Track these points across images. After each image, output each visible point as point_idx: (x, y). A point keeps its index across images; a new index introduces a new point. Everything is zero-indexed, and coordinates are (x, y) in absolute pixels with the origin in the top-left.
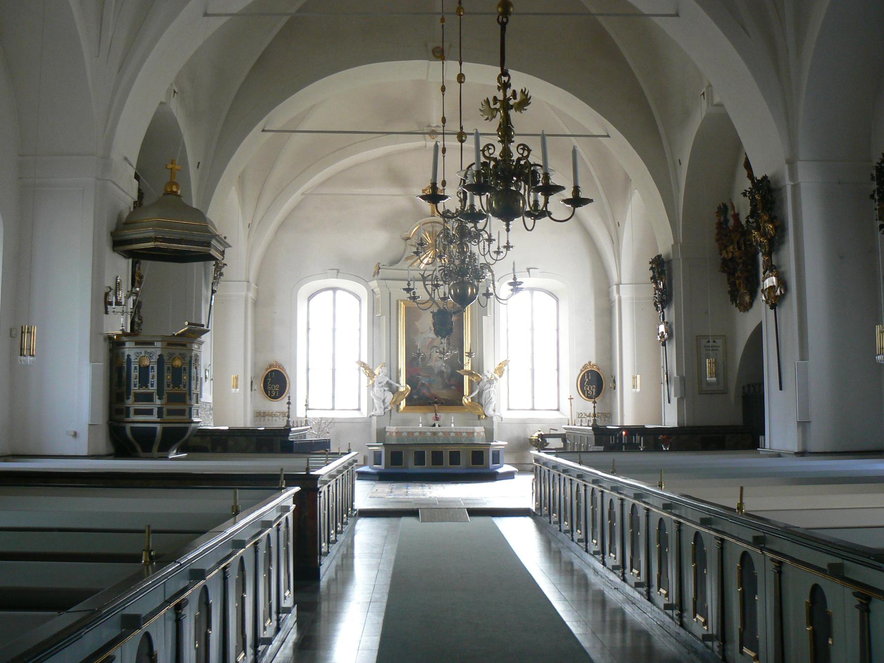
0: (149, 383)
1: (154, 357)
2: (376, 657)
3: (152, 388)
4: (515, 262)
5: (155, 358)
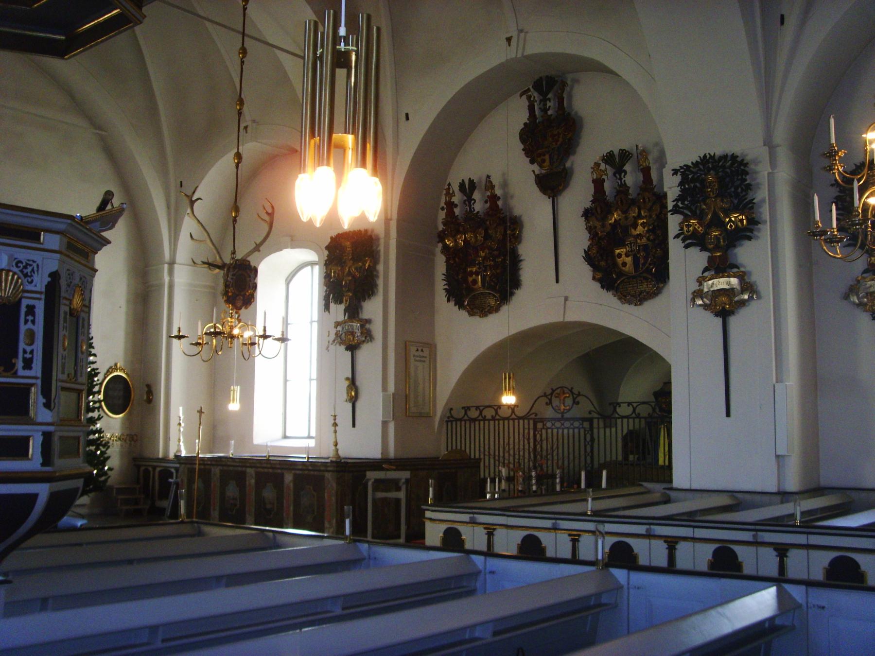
0: (17, 357)
1: (36, 278)
2: (259, 584)
3: (27, 373)
4: (266, 311)
5: (40, 282)
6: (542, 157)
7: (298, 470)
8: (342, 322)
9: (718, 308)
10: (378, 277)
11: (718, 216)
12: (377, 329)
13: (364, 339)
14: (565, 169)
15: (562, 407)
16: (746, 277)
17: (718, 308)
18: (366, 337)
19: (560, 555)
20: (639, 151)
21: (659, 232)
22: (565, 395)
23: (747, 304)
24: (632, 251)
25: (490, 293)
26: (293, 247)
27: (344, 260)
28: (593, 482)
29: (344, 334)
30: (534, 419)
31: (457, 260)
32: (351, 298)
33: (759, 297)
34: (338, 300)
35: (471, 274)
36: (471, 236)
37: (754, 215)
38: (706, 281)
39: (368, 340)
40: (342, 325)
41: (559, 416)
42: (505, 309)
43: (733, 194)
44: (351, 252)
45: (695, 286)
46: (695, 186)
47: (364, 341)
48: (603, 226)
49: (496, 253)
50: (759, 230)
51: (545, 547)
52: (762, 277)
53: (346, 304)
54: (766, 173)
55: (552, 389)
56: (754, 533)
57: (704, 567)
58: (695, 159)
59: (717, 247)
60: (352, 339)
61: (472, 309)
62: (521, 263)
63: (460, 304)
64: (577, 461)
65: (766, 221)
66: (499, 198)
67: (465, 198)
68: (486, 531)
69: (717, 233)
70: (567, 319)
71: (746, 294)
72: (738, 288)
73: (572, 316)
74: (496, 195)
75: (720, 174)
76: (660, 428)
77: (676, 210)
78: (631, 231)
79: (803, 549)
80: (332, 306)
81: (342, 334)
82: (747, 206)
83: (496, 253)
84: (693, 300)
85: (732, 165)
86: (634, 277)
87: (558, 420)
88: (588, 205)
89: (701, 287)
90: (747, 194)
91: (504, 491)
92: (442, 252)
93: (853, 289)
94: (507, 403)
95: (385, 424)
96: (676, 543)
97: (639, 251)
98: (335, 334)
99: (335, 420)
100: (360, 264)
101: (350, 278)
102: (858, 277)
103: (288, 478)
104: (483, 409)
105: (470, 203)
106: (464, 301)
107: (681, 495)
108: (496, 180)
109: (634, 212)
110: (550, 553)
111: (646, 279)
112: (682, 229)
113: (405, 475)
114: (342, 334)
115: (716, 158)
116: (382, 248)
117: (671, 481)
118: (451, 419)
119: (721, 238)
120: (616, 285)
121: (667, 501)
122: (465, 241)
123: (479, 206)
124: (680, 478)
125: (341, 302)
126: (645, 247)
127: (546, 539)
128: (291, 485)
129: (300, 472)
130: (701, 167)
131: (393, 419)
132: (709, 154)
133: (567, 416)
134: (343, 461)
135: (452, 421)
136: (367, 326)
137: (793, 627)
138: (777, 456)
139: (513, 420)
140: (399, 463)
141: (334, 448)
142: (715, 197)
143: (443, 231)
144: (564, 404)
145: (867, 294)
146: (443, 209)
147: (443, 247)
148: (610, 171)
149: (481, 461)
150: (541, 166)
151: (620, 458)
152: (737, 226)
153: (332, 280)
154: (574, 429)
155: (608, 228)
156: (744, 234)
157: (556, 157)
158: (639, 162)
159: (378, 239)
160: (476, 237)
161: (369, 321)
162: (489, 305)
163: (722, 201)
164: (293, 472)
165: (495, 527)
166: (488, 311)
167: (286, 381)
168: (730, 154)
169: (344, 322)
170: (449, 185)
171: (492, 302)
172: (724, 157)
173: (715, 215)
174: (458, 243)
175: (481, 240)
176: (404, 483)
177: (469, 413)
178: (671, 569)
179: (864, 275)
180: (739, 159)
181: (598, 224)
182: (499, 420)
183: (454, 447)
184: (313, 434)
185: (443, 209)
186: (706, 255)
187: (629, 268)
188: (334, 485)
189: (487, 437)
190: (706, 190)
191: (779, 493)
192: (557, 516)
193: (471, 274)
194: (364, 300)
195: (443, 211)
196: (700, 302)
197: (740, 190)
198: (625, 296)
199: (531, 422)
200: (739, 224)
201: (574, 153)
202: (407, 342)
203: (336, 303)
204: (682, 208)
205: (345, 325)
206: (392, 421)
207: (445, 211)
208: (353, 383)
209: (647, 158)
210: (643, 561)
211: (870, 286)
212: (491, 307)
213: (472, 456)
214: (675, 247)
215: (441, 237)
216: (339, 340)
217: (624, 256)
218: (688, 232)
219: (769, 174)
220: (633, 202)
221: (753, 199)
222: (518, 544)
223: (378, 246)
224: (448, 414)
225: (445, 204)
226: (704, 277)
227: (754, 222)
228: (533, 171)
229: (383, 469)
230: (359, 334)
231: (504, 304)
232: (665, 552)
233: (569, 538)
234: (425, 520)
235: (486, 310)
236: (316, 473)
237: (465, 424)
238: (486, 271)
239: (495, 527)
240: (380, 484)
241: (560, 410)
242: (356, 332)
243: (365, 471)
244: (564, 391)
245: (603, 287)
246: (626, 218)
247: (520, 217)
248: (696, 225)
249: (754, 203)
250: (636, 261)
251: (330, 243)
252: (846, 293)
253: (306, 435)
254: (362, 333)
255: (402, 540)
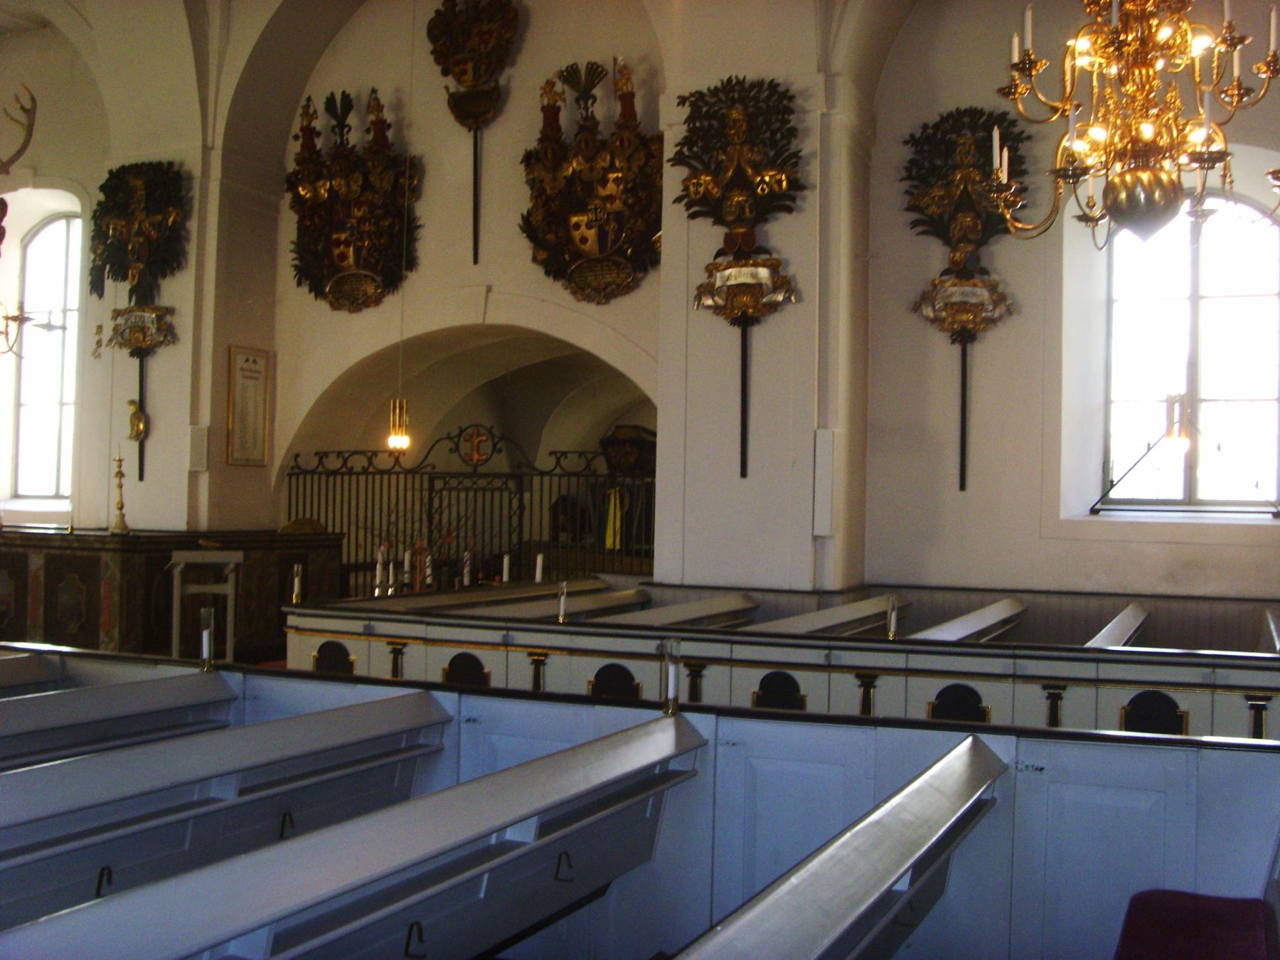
6: (462, 67)
7: (55, 547)
8: (126, 310)
9: (736, 312)
10: (188, 240)
11: (743, 173)
12: (184, 323)
13: (161, 339)
14: (497, 88)
15: (476, 457)
16: (781, 268)
17: (736, 312)
18: (165, 337)
19: (514, 684)
20: (617, 68)
21: (642, 194)
22: (480, 438)
23: (779, 309)
24: (596, 220)
25: (366, 276)
26: (36, 185)
27: (130, 211)
28: (522, 571)
29: (128, 331)
30: (430, 474)
31: (316, 220)
32: (141, 273)
33: (799, 300)
34: (120, 275)
35: (338, 243)
36: (340, 184)
37: (799, 175)
38: (719, 271)
39: (169, 341)
40: (126, 316)
41: (470, 470)
42: (391, 301)
43: (768, 142)
44: (144, 196)
45: (702, 278)
46: (711, 126)
47: (161, 343)
48: (554, 179)
49: (380, 212)
50: (804, 199)
51: (638, 684)
52: (804, 270)
53: (133, 280)
54: (819, 113)
55: (460, 428)
56: (827, 652)
57: (745, 701)
58: (714, 82)
59: (740, 220)
60: (141, 337)
61: (338, 299)
62: (419, 230)
63: (318, 291)
64: (496, 541)
65: (816, 187)
66: (389, 126)
67: (334, 123)
68: (390, 648)
69: (741, 199)
70: (489, 321)
71: (780, 293)
72: (769, 283)
73: (499, 316)
74: (385, 121)
75: (751, 110)
76: (610, 494)
77: (678, 160)
78: (597, 189)
79: (725, 665)
80: (109, 284)
81: (124, 330)
82: (790, 161)
83: (380, 212)
84: (698, 298)
85: (769, 97)
86: (597, 261)
87: (466, 475)
88: (532, 144)
89: (712, 280)
90: (788, 143)
91: (404, 585)
92: (292, 207)
93: (927, 297)
94: (395, 447)
95: (193, 476)
96: (703, 667)
97: (607, 221)
98: (114, 330)
99: (120, 466)
100: (159, 218)
101: (141, 240)
102: (935, 280)
103: (36, 561)
104: (349, 456)
105: (342, 131)
106: (325, 286)
107: (669, 594)
108: (385, 97)
109: (604, 160)
110: (813, 707)
111: (617, 264)
112: (686, 189)
113: (233, 558)
114: (124, 330)
115: (747, 85)
116: (196, 193)
117: (651, 574)
118: (296, 471)
119: (747, 205)
120: (569, 271)
121: (644, 603)
122: (330, 190)
123: (356, 137)
124: (666, 566)
125: (124, 278)
126: (618, 215)
127: (492, 661)
128: (42, 573)
129: (58, 552)
130: (722, 96)
131: (208, 468)
132: (736, 77)
133: (482, 469)
134: (131, 534)
135: (297, 475)
136: (168, 318)
137: (994, 800)
138: (815, 538)
139: (343, 474)
140: (223, 539)
141: (117, 512)
142: (742, 144)
143: (295, 173)
144: (478, 451)
145: (946, 305)
146: (296, 137)
147: (293, 198)
148: (570, 94)
149: (344, 538)
150: (458, 79)
151: (546, 537)
152: (771, 189)
153: (109, 241)
154: (476, 491)
155: (562, 183)
156: (782, 202)
157: (484, 67)
158: (616, 84)
159: (190, 178)
160: (349, 186)
161: (170, 311)
162: (366, 294)
163: (752, 150)
164: (45, 551)
165: (405, 641)
166: (363, 303)
167: (18, 405)
168: (767, 80)
169: (128, 310)
170: (309, 99)
171: (370, 289)
172: (759, 85)
173: (740, 172)
174: (319, 192)
175: (356, 192)
176: (232, 571)
177: (564, 462)
178: (537, 694)
179: (944, 278)
180: (781, 89)
181: (547, 177)
182: (374, 474)
183: (301, 515)
184: (66, 489)
185: (296, 137)
186: (721, 231)
187: (591, 245)
188: (118, 575)
189: (331, 496)
190: (729, 132)
191: (814, 592)
192: (510, 625)
193: (338, 243)
194: (164, 277)
195: (297, 142)
196: (709, 302)
197: (778, 136)
198: (583, 289)
199: (426, 478)
200: (776, 187)
201: (513, 63)
202: (233, 349)
203: (115, 280)
204: (688, 157)
205: (130, 315)
206: (205, 471)
207: (301, 141)
208: (141, 408)
209: (629, 80)
210: (496, 682)
211: (952, 295)
212: (368, 297)
213: (330, 529)
214: (673, 217)
215: (292, 183)
216: (120, 339)
217: (583, 227)
218: (696, 193)
219: (822, 115)
220: (603, 146)
221: (800, 152)
222: (444, 669)
223: (190, 189)
224: (292, 463)
225: (302, 129)
226: (717, 264)
227: (797, 186)
228: (447, 88)
229: (199, 548)
230: (154, 331)
231: (388, 293)
232: (529, 671)
233: (529, 660)
234: (288, 630)
235: (360, 301)
236: (85, 553)
237: (320, 479)
238: (362, 240)
239: (405, 641)
240: (194, 572)
241: (471, 460)
242: (149, 328)
243: (171, 551)
244: (478, 432)
245: (548, 273)
246: (592, 169)
247: (421, 158)
248: (709, 184)
249: (800, 158)
250: (602, 236)
251: (108, 180)
252: (916, 303)
253: (52, 493)
254: (159, 329)
255: (175, 654)
